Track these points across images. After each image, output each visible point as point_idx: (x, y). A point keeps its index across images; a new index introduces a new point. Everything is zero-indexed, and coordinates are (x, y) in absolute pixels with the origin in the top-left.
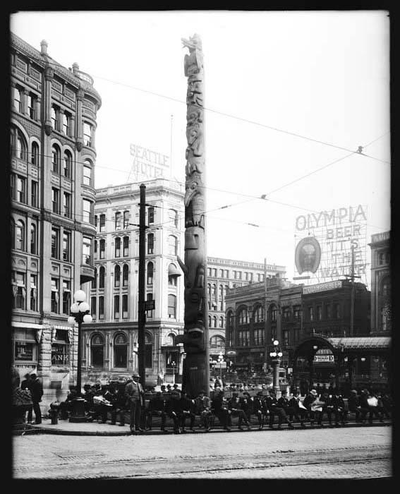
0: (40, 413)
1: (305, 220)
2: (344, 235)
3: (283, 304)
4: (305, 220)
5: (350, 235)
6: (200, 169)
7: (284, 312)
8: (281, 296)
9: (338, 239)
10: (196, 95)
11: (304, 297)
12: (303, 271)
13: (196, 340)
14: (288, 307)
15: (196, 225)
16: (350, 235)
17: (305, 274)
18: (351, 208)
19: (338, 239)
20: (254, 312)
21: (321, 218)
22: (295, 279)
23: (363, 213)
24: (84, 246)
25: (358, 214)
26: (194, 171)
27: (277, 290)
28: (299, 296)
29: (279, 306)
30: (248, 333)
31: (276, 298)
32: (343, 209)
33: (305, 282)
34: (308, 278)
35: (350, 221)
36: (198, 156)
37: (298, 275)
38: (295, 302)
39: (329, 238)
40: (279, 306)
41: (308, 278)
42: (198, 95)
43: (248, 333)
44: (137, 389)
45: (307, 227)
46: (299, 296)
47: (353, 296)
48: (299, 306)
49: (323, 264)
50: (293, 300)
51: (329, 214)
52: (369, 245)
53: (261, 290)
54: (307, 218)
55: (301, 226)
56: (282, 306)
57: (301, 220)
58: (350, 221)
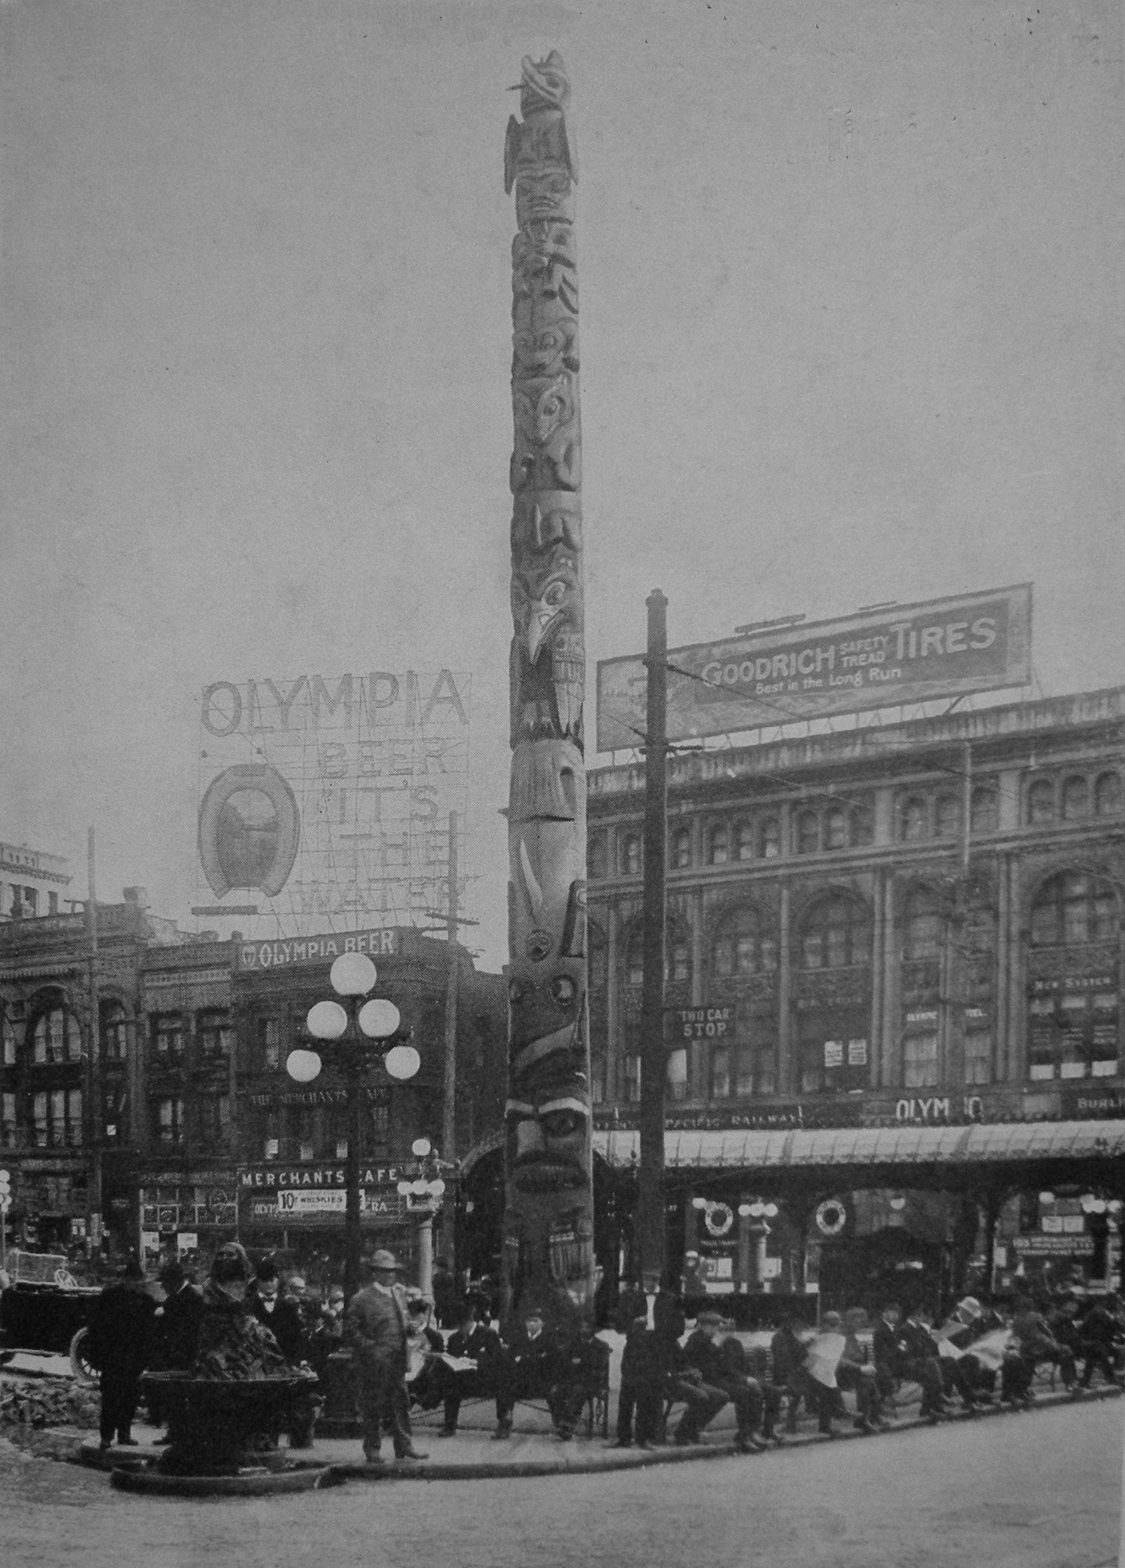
0: (710, 1419)
1: (237, 699)
2: (385, 771)
3: (152, 1001)
4: (237, 699)
5: (408, 772)
6: (575, 537)
7: (156, 1032)
8: (142, 973)
9: (363, 783)
10: (560, 270)
11: (243, 979)
12: (230, 885)
13: (570, 1139)
14: (174, 1014)
15: (565, 736)
16: (408, 772)
17: (238, 897)
18: (410, 672)
19: (363, 783)
20: (32, 1024)
21: (425, 702)
22: (196, 911)
23: (455, 699)
24: (976, 827)
25: (436, 699)
26: (557, 541)
27: (128, 950)
28: (223, 975)
29: (138, 1011)
30: (76, 1097)
31: (126, 979)
32: (382, 676)
33: (252, 929)
34: (251, 910)
35: (410, 724)
36: (567, 487)
37: (208, 899)
38: (201, 999)
39: (333, 776)
40: (138, 1011)
41: (251, 910)
42: (568, 272)
43: (76, 1097)
44: (392, 1315)
45: (244, 724)
46: (223, 975)
47: (451, 988)
48: (223, 1012)
49: (305, 868)
50: (196, 991)
51: (332, 688)
52: (505, 812)
53: (69, 942)
54: (244, 693)
55: (219, 721)
56: (149, 1007)
57: (223, 698)
58: (410, 724)
